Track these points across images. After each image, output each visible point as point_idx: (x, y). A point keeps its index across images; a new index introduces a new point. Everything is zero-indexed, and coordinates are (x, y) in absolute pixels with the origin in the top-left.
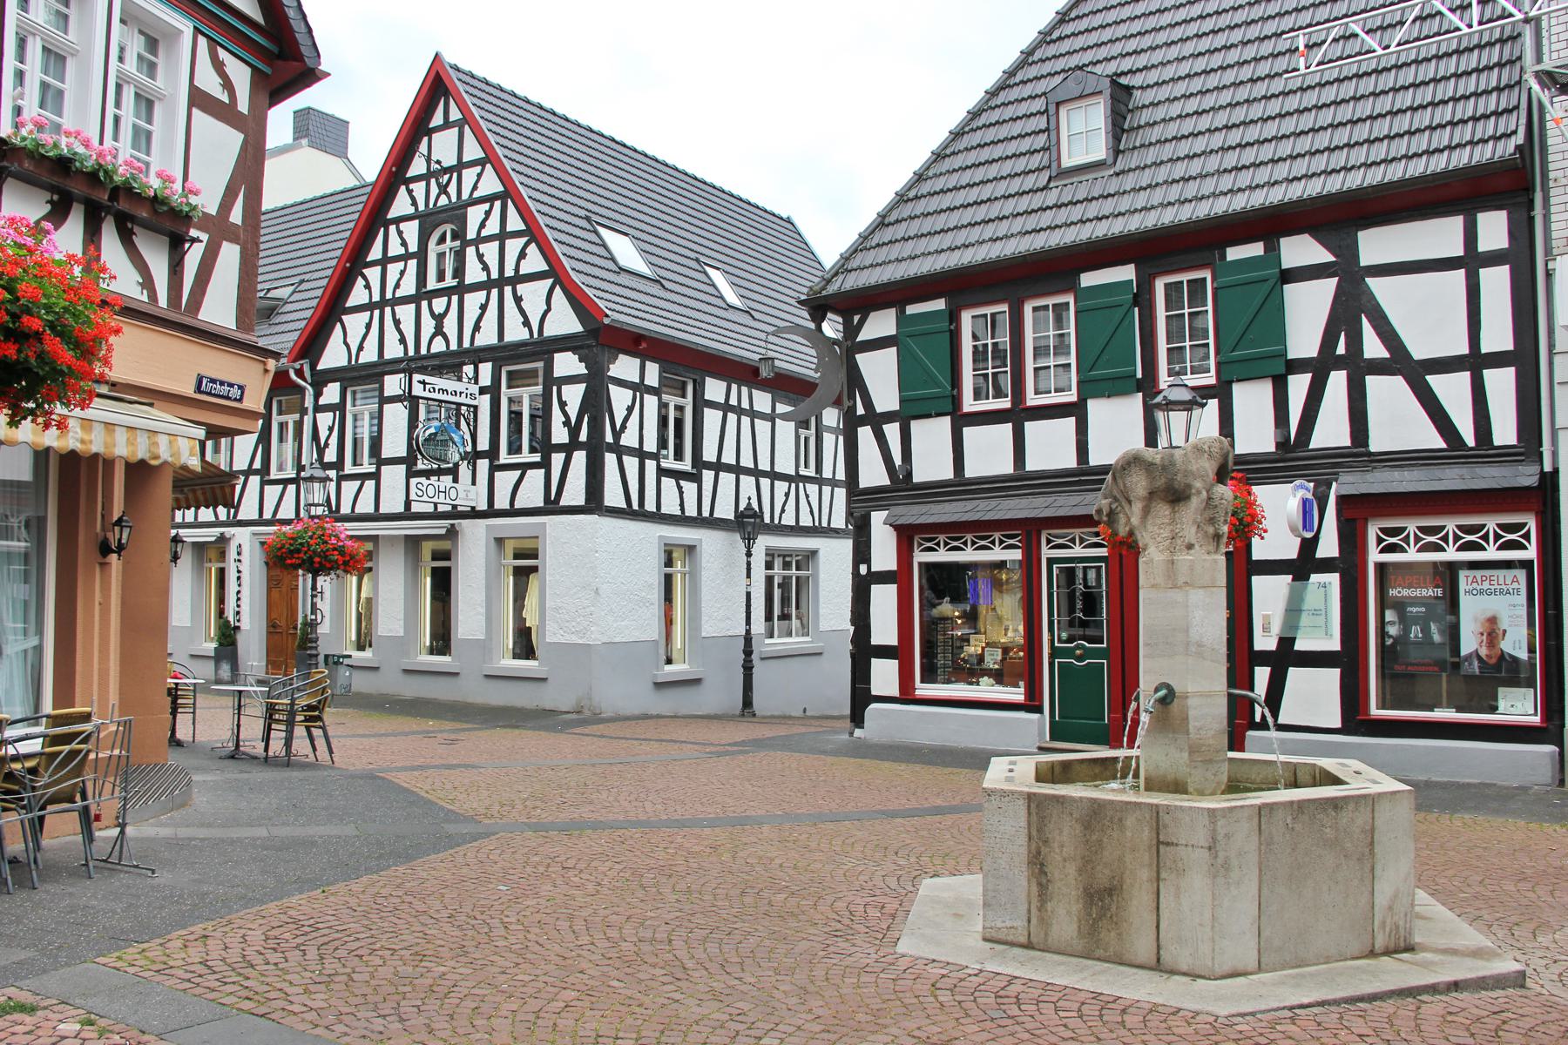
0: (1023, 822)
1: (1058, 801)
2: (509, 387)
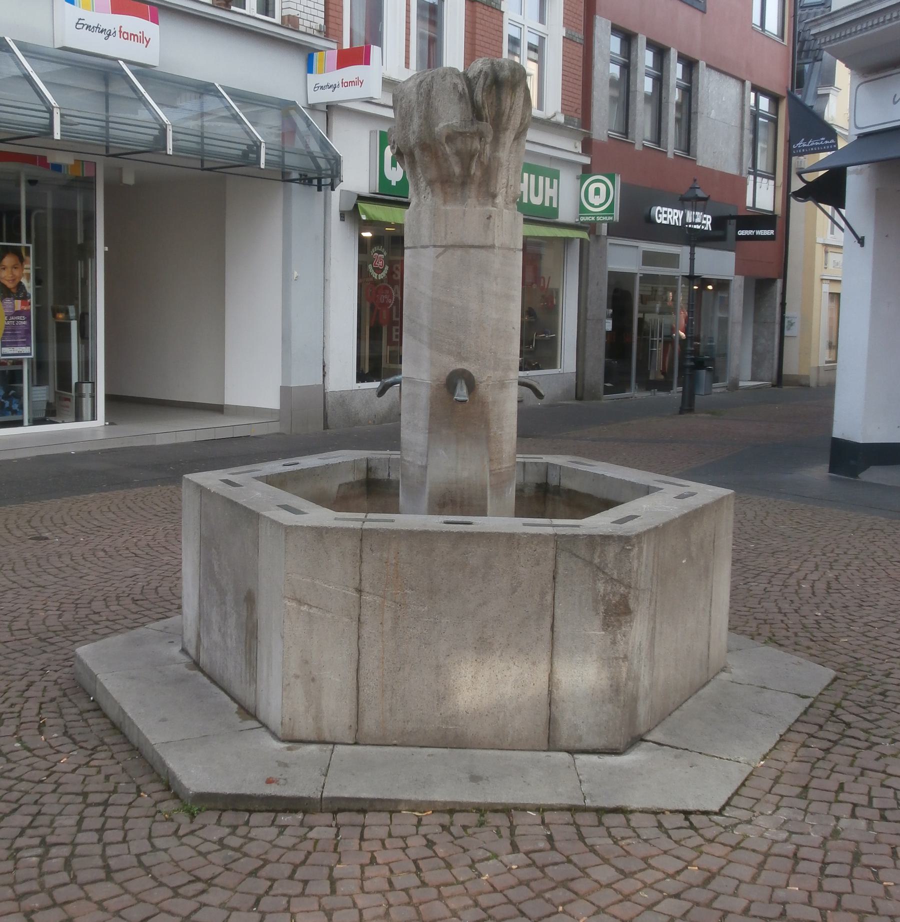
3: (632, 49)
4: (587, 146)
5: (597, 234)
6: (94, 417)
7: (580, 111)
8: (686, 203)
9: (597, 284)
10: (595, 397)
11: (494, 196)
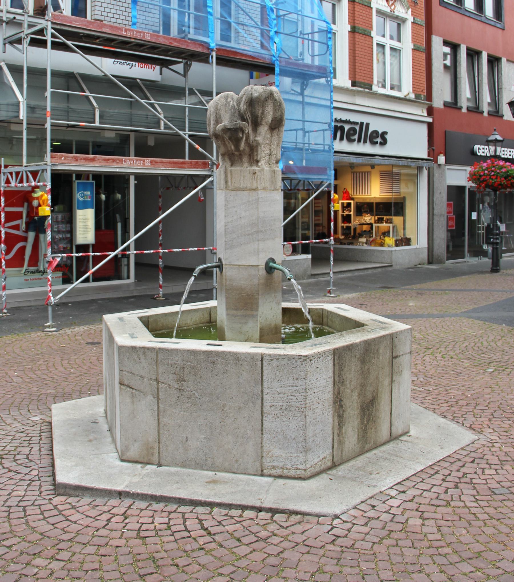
0: (331, 374)
1: (349, 349)
3: (458, 53)
4: (430, 111)
5: (439, 163)
6: (128, 278)
7: (425, 91)
8: (489, 143)
9: (440, 193)
10: (440, 262)
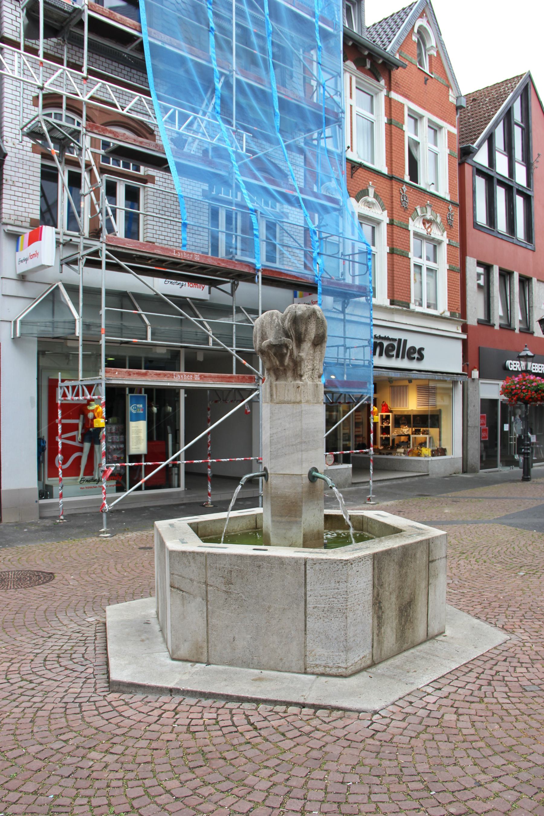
0: (370, 578)
2: (275, 262)
4: (465, 327)
6: (179, 486)
7: (460, 309)
10: (474, 471)
11: (301, 376)
